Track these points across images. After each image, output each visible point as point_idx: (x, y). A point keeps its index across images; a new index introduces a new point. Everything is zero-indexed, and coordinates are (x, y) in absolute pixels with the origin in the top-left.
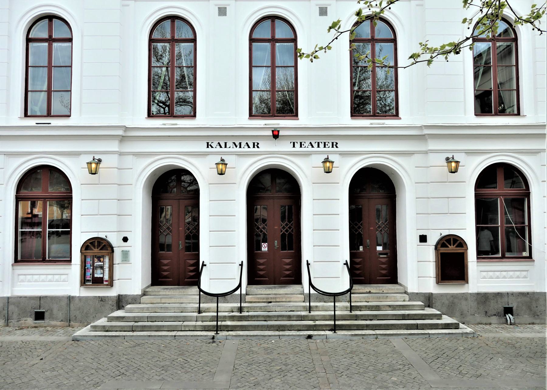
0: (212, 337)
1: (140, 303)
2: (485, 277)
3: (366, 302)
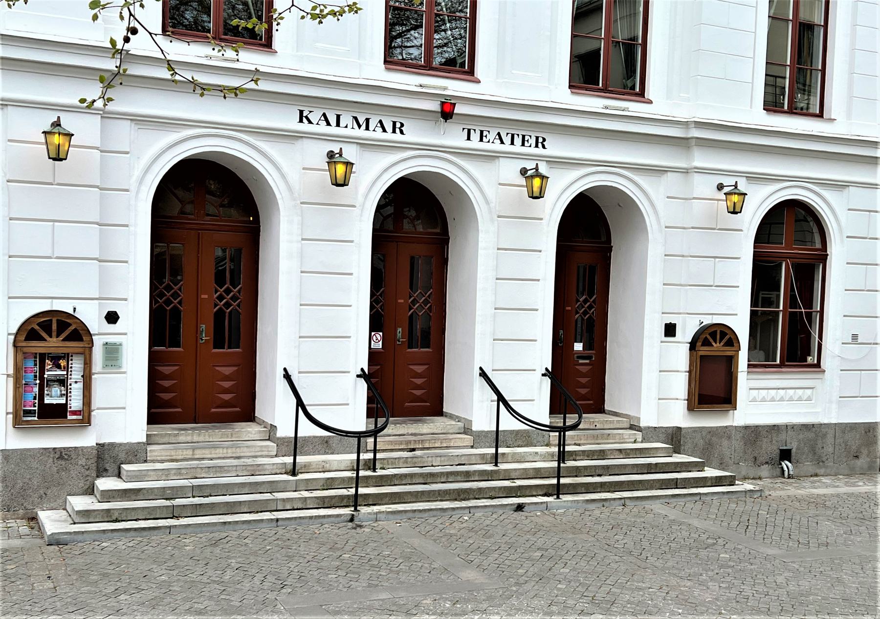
0: (349, 518)
1: (146, 461)
2: (764, 400)
3: (575, 444)
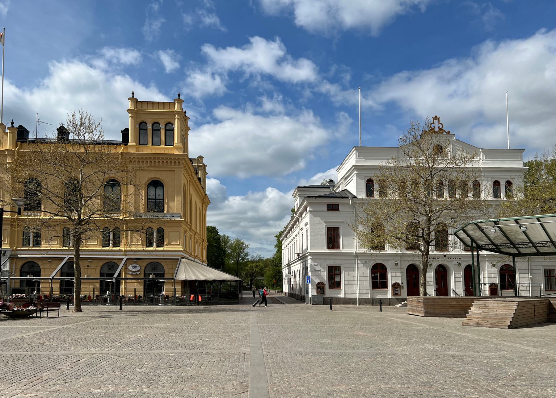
2: (330, 293)
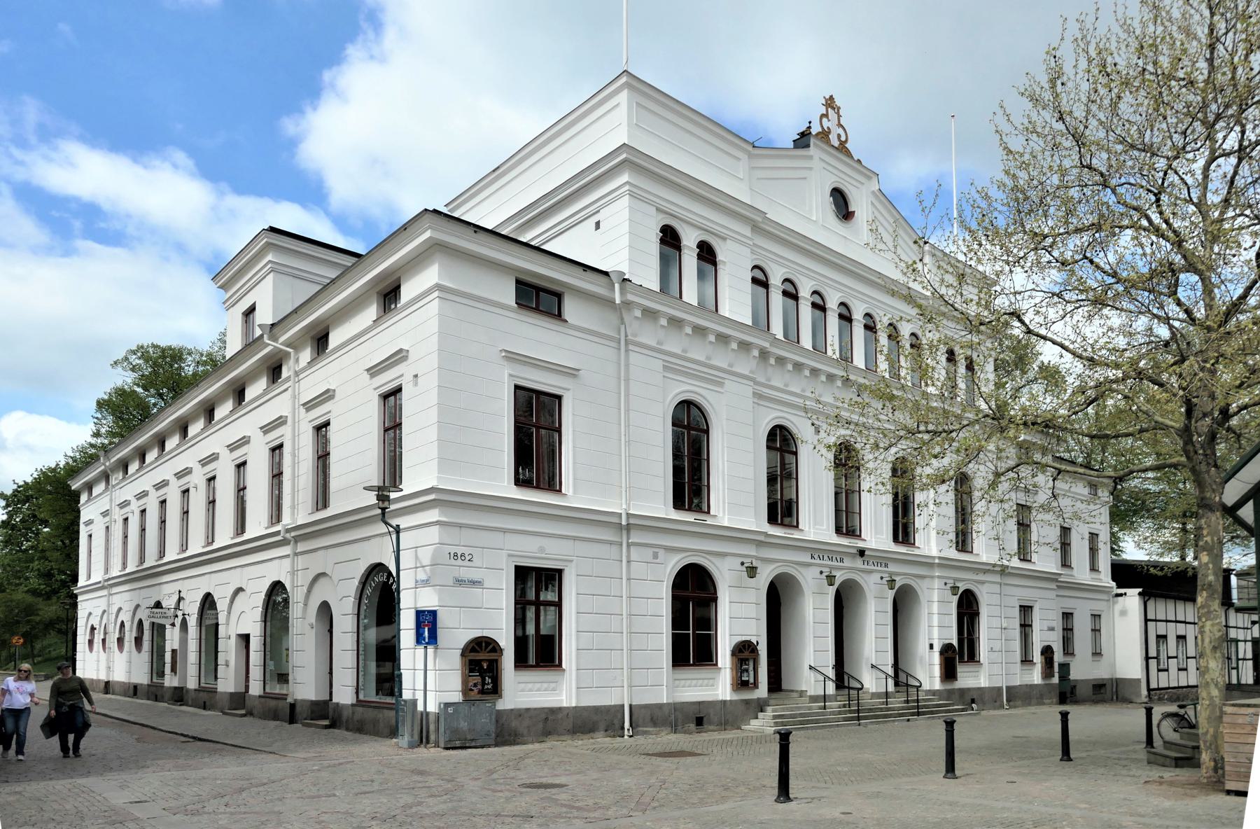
2: (522, 691)
